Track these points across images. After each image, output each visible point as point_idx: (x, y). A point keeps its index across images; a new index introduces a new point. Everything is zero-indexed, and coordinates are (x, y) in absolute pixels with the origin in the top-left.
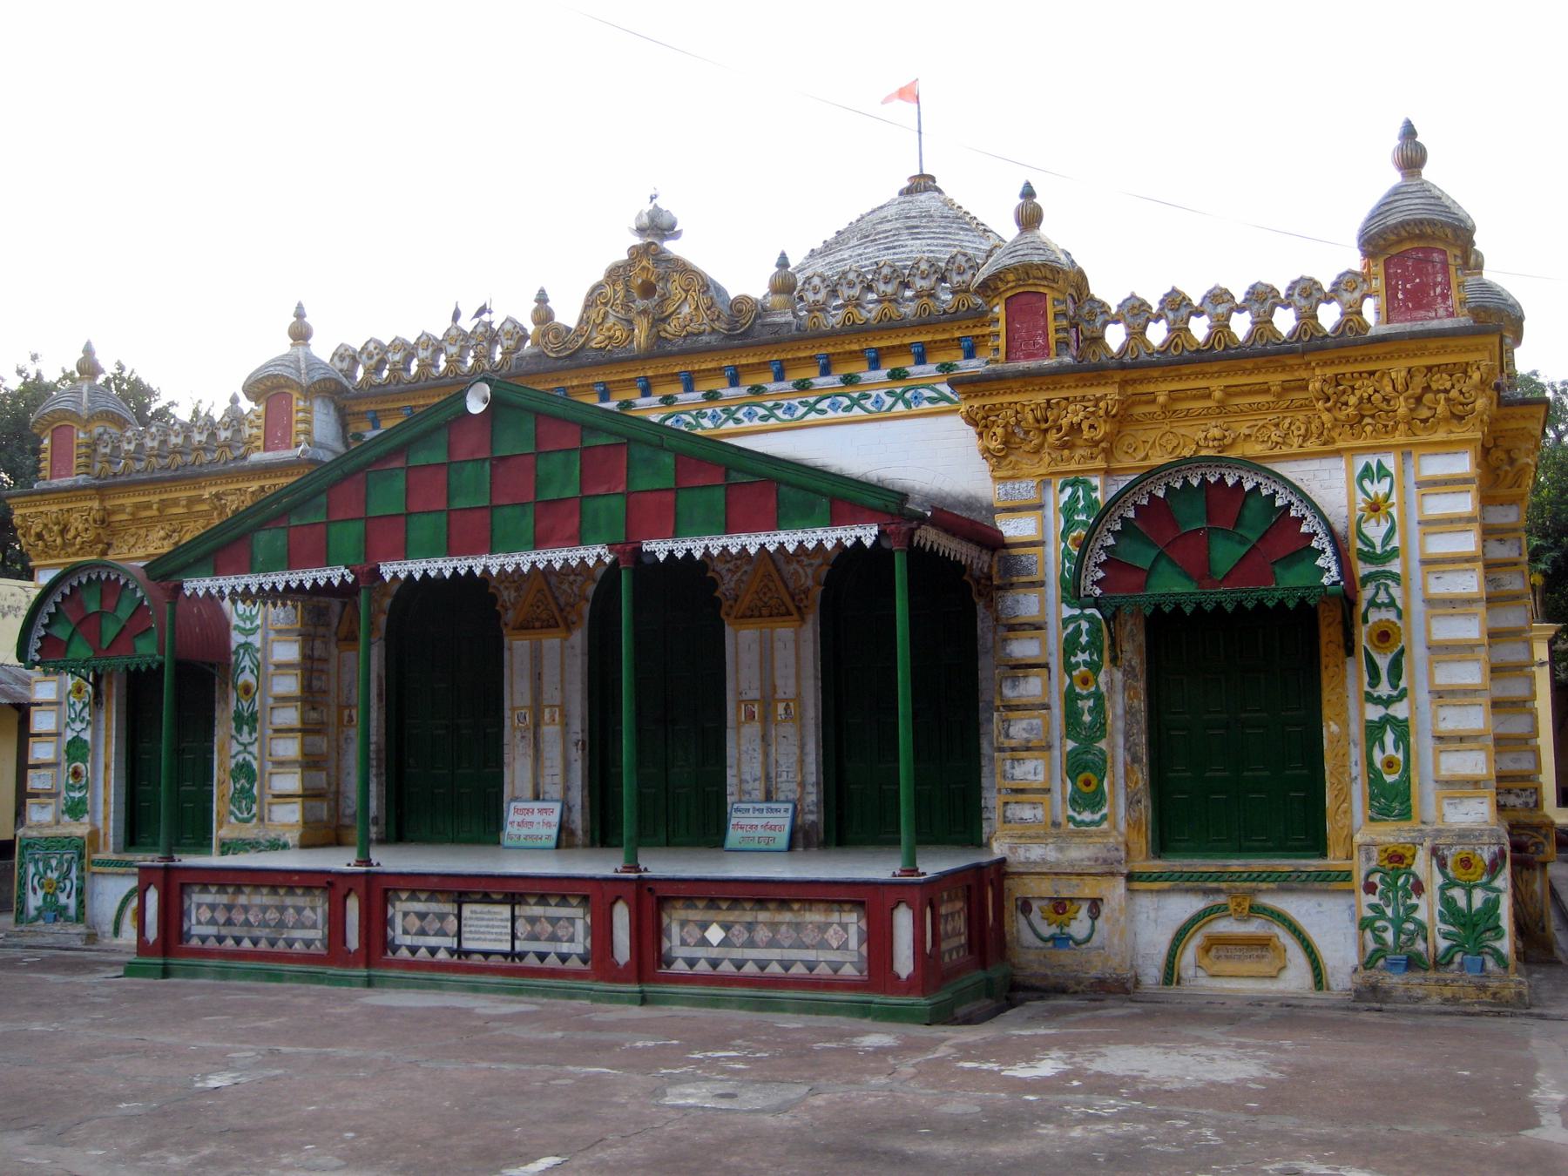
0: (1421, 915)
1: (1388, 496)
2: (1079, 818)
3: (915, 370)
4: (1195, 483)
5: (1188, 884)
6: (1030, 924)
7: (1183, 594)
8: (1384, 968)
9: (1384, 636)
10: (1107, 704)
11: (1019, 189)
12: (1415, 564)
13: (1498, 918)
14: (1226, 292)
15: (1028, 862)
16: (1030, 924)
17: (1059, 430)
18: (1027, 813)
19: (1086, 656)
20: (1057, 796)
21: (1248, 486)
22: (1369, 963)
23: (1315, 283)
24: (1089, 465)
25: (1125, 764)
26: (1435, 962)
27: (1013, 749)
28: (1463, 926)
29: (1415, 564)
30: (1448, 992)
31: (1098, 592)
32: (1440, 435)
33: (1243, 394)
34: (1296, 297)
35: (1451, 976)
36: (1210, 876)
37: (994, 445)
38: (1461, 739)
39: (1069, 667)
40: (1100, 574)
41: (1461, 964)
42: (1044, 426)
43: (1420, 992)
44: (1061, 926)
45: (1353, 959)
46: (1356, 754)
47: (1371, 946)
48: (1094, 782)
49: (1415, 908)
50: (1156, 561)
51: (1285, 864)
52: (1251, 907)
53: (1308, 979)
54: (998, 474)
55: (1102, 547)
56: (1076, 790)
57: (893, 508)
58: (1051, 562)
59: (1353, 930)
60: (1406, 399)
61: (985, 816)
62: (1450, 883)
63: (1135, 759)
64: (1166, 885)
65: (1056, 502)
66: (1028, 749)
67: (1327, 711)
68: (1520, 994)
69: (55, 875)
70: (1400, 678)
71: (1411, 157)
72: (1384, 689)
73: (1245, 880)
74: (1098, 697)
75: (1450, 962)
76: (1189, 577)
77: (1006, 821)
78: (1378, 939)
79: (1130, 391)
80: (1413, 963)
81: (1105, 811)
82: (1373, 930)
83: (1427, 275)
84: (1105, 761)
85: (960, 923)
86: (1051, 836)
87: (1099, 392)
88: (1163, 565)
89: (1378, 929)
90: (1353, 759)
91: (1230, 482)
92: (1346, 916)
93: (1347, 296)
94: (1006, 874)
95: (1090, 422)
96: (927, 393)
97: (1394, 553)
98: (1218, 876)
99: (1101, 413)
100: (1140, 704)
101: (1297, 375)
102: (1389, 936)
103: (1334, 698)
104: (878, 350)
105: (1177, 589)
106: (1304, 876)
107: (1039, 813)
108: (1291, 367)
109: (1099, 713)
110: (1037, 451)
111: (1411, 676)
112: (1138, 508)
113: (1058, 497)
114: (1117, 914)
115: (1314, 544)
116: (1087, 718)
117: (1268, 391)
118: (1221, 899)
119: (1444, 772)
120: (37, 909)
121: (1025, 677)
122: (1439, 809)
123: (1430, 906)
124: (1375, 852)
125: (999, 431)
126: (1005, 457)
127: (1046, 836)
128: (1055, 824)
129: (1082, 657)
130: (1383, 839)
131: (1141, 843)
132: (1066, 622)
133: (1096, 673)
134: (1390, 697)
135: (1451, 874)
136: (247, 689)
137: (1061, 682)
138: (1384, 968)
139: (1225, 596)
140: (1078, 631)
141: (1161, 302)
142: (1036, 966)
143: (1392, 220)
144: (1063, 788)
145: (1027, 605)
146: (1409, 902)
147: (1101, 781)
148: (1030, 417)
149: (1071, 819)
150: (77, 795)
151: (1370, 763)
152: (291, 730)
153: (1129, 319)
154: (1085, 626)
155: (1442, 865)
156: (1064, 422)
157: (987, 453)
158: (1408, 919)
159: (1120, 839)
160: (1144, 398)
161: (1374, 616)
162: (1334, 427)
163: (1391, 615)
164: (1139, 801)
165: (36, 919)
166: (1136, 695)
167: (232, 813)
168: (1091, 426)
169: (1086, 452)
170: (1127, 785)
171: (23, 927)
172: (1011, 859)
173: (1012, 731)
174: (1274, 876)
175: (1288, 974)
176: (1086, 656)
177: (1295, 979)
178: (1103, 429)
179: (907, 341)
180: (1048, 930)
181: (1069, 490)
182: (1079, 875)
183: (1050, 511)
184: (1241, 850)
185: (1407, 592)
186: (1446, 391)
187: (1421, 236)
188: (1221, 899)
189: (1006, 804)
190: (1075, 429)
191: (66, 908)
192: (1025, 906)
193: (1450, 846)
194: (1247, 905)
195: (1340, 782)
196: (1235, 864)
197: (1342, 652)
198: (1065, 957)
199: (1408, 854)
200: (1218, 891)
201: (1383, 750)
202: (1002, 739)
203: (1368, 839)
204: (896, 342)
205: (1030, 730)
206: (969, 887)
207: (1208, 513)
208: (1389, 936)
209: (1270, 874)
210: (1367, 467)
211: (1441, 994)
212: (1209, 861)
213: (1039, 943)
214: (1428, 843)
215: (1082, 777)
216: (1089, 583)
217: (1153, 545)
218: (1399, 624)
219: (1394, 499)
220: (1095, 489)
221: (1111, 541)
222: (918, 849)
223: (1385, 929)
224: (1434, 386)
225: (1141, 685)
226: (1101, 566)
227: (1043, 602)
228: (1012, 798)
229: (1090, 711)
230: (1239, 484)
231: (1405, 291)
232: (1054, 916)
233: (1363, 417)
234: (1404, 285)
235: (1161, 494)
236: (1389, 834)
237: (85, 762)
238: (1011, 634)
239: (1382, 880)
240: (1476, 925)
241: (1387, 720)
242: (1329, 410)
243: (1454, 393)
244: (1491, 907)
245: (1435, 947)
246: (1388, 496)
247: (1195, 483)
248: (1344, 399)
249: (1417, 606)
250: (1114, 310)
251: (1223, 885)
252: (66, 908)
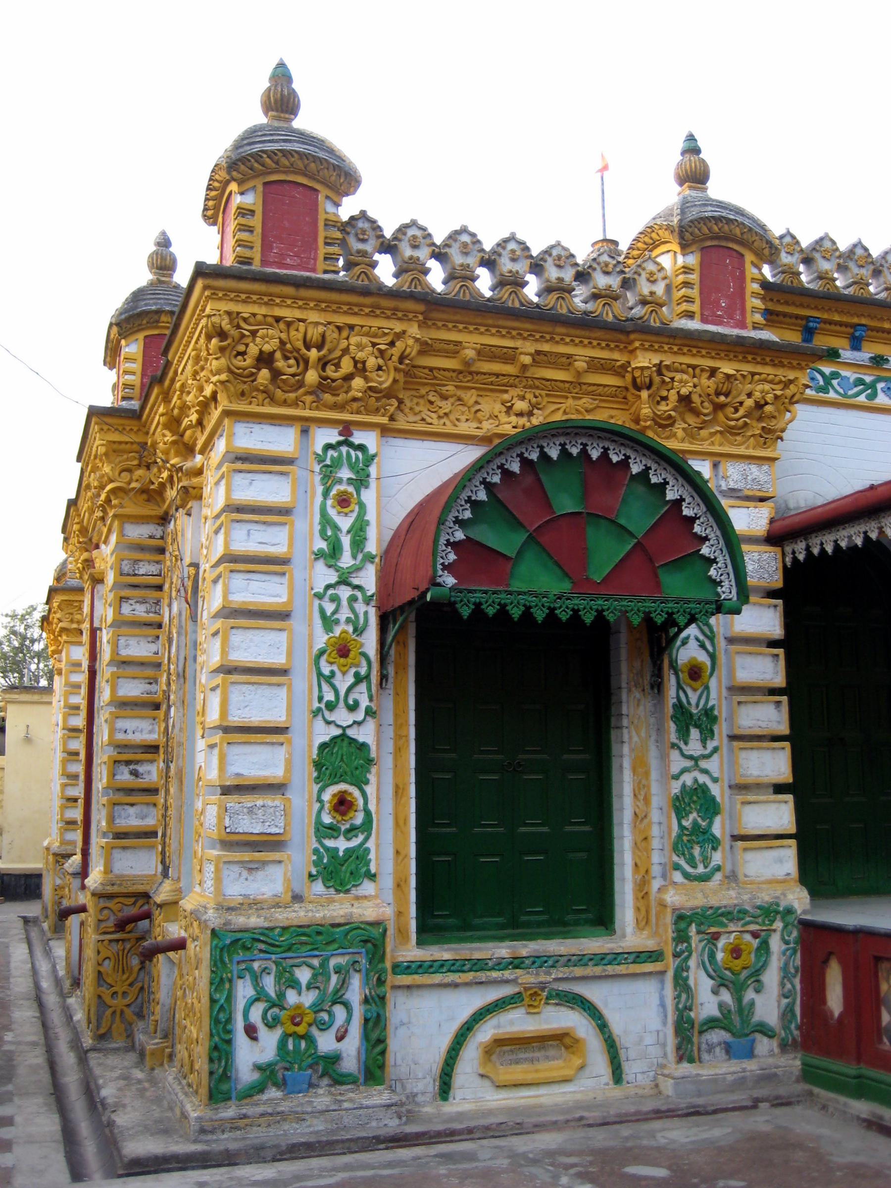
69: (308, 999)
71: (695, 175)
120: (258, 1068)
136: (695, 672)
150: (342, 845)
152: (776, 738)
165: (259, 1088)
167: (677, 867)
171: (230, 1111)
191: (334, 1059)
237: (360, 783)
252: (334, 1059)
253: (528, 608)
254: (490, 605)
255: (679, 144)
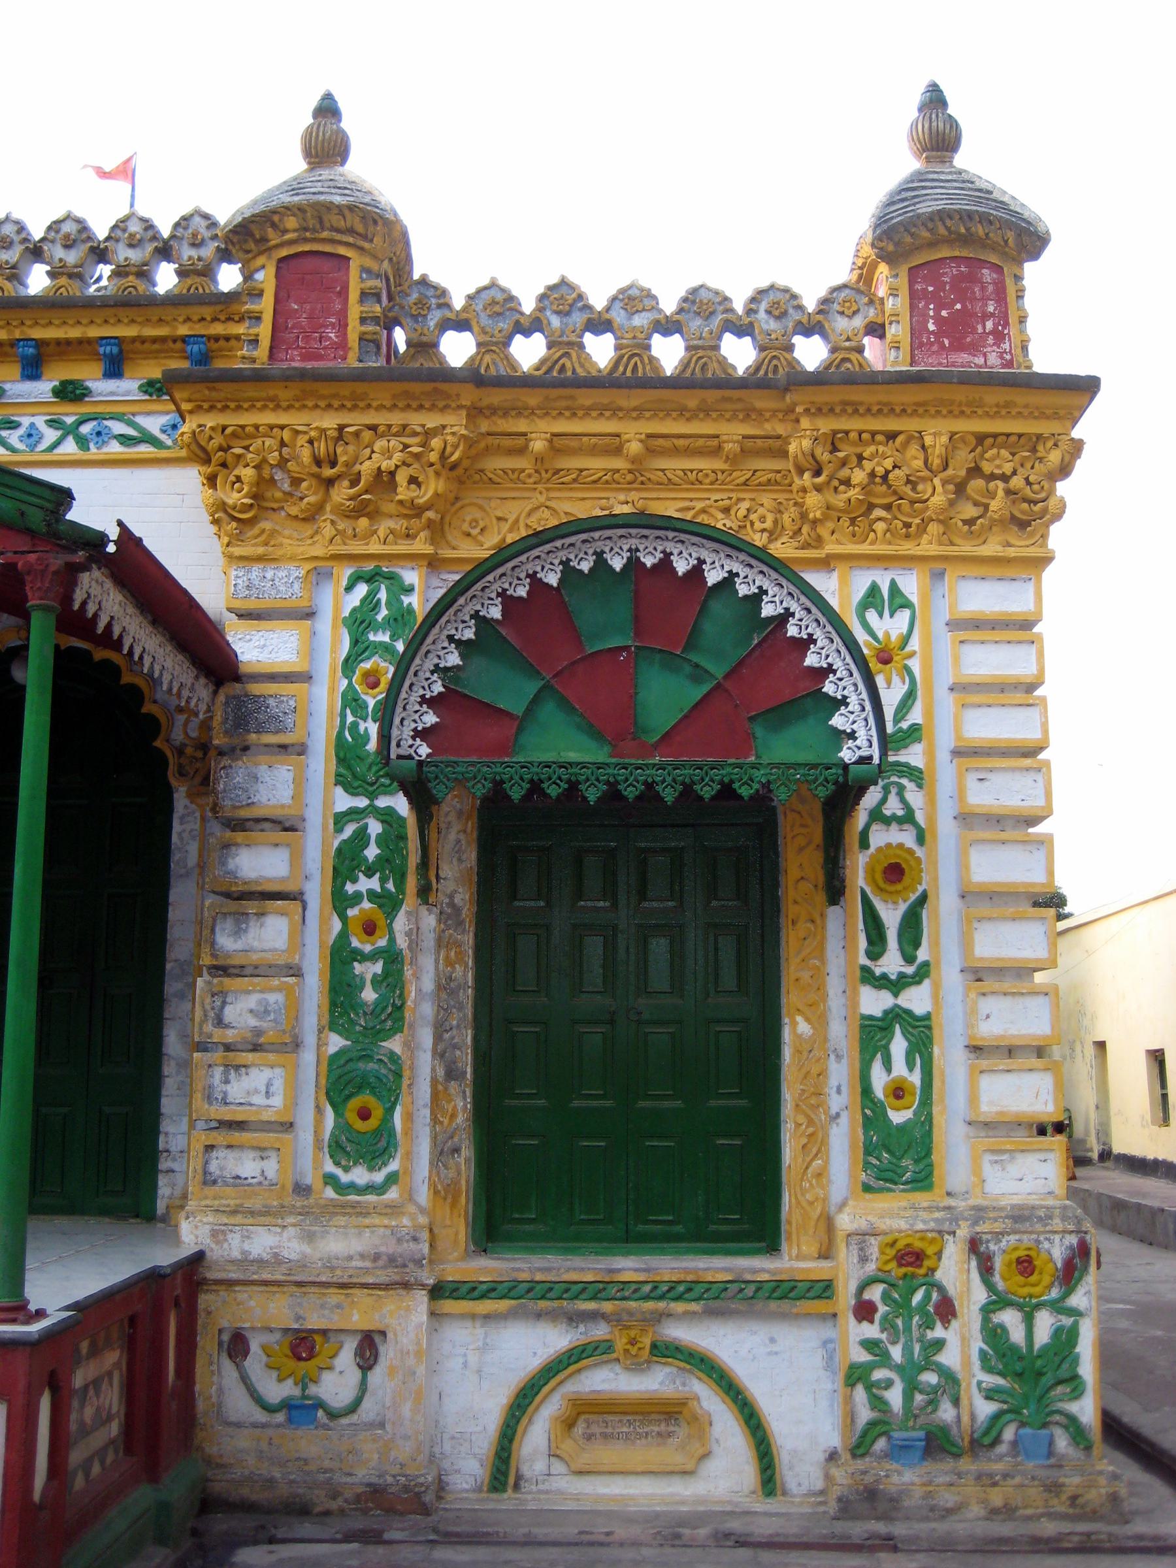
0: (949, 1358)
1: (905, 640)
2: (345, 1178)
3: (102, 387)
4: (617, 564)
5: (543, 1304)
6: (245, 1379)
7: (583, 765)
8: (886, 1455)
9: (894, 872)
10: (408, 972)
11: (314, 101)
12: (943, 756)
13: (1076, 1361)
14: (649, 295)
15: (245, 1261)
16: (245, 1379)
17: (355, 482)
18: (248, 1166)
19: (374, 883)
20: (305, 1136)
21: (713, 577)
22: (860, 1447)
23: (794, 297)
24: (402, 548)
25: (434, 1082)
26: (973, 1442)
27: (228, 1048)
28: (1019, 1375)
29: (943, 756)
30: (997, 1498)
31: (424, 750)
32: (991, 548)
33: (676, 452)
34: (762, 315)
35: (998, 1467)
36: (583, 1290)
37: (234, 498)
38: (1011, 1051)
39: (341, 902)
40: (431, 719)
41: (1015, 1444)
42: (328, 472)
43: (948, 1498)
44: (304, 1382)
45: (832, 1437)
46: (840, 1073)
47: (865, 1414)
48: (378, 1113)
49: (939, 1344)
50: (536, 700)
51: (716, 1266)
52: (654, 1346)
53: (747, 1473)
54: (237, 551)
55: (436, 669)
56: (342, 1126)
57: (36, 518)
58: (319, 713)
59: (829, 1384)
60: (944, 483)
61: (163, 1165)
62: (998, 1302)
63: (452, 1074)
64: (504, 1305)
65: (337, 608)
66: (256, 1048)
67: (790, 998)
68: (1114, 1498)
70: (917, 945)
71: (938, 137)
72: (891, 963)
73: (647, 1298)
74: (392, 958)
75: (997, 1441)
76: (596, 732)
77: (209, 1181)
78: (877, 1403)
79: (484, 426)
80: (937, 1444)
81: (394, 1166)
82: (869, 1387)
83: (973, 299)
84: (398, 1075)
85: (112, 1397)
86: (293, 1211)
87: (432, 421)
88: (549, 711)
89: (876, 1384)
90: (833, 1082)
91: (681, 567)
92: (818, 1360)
93: (841, 324)
94: (204, 1281)
95: (411, 471)
96: (118, 428)
97: (914, 734)
98: (598, 1290)
99: (433, 457)
100: (465, 974)
101: (768, 428)
102: (895, 1397)
103: (805, 975)
104: (40, 344)
105: (573, 756)
106: (750, 1290)
107: (271, 1167)
108: (760, 413)
109: (392, 987)
110: (311, 517)
111: (935, 944)
112: (508, 602)
113: (340, 599)
114: (411, 1361)
115: (829, 688)
116: (369, 995)
117: (716, 452)
118: (600, 1331)
119: (988, 1107)
121: (261, 914)
122: (977, 1170)
123: (965, 1341)
124: (874, 1247)
125: (248, 473)
126: (252, 522)
127: (282, 1211)
128: (302, 1190)
129: (366, 884)
130: (885, 1224)
131: (457, 1228)
132: (341, 819)
133: (391, 914)
134: (902, 976)
135: (1001, 1286)
137: (324, 923)
138: (886, 1455)
139: (665, 774)
140: (361, 837)
141: (542, 298)
142: (251, 1461)
143: (925, 208)
144: (316, 1121)
145: (272, 785)
146: (930, 1335)
147: (390, 1111)
148: (306, 454)
149: (330, 1179)
151: (866, 1090)
153: (485, 320)
154: (375, 828)
155: (986, 1270)
156: (366, 468)
157: (221, 514)
158: (928, 1365)
159: (423, 1220)
160: (507, 442)
161: (879, 837)
162: (826, 517)
163: (906, 838)
164: (456, 1150)
166: (460, 959)
168: (413, 480)
169: (399, 525)
170: (435, 1120)
172: (215, 1253)
173: (230, 1013)
174: (699, 1289)
175: (713, 1466)
176: (374, 883)
177: (723, 1475)
178: (433, 486)
179: (94, 332)
180: (276, 1390)
181: (362, 589)
182: (343, 1286)
183: (325, 624)
184: (631, 1238)
185: (931, 801)
186: (1005, 478)
187: (966, 240)
188: (600, 1331)
189: (210, 1148)
190: (385, 481)
192: (237, 1345)
193: (998, 1236)
194: (647, 1341)
195: (811, 1122)
196: (629, 1266)
197: (821, 897)
198: (309, 1444)
199: (930, 1251)
200: (594, 1316)
201: (888, 1065)
202: (209, 1027)
203: (862, 1224)
204: (74, 333)
205: (262, 1012)
206: (132, 1320)
207: (637, 619)
208: (895, 1397)
209: (691, 1286)
210: (874, 590)
211: (984, 1502)
212: (577, 1261)
213: (260, 1416)
214: (963, 1232)
215: (355, 1103)
216: (407, 732)
217: (533, 672)
218: (919, 852)
219: (914, 644)
220: (410, 590)
221: (453, 659)
222: (35, 1224)
223: (889, 1384)
224: (987, 468)
225: (468, 940)
226: (431, 702)
227: (300, 782)
228: (220, 1138)
229: (377, 982)
230: (697, 572)
231: (939, 320)
232: (291, 1364)
233: (871, 507)
234: (937, 310)
235: (553, 579)
236: (897, 1214)
238: (239, 837)
239: (886, 1297)
240: (1040, 1374)
241: (896, 1015)
242: (818, 489)
243: (1017, 482)
244: (1065, 1340)
245: (973, 1417)
246: (905, 640)
247: (617, 564)
248: (844, 473)
249: (946, 828)
250: (458, 303)
251: (607, 1307)
253: (649, 786)
254: (707, 784)
255: (915, 96)
